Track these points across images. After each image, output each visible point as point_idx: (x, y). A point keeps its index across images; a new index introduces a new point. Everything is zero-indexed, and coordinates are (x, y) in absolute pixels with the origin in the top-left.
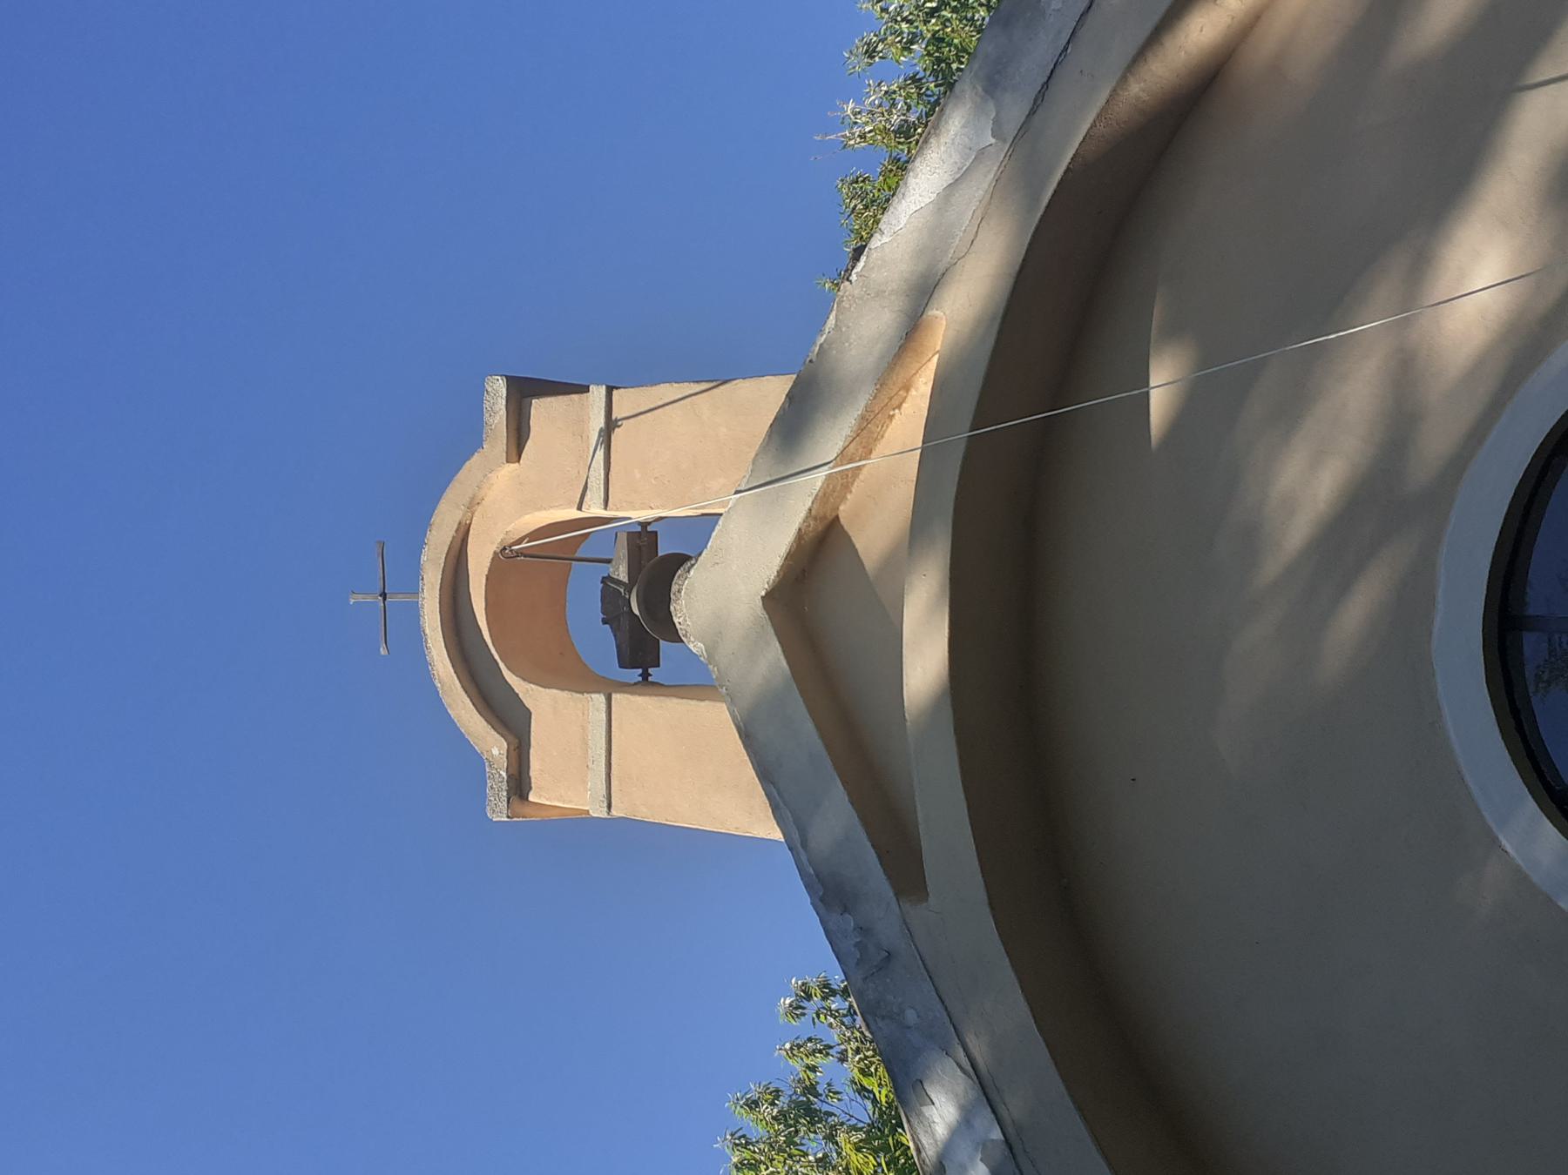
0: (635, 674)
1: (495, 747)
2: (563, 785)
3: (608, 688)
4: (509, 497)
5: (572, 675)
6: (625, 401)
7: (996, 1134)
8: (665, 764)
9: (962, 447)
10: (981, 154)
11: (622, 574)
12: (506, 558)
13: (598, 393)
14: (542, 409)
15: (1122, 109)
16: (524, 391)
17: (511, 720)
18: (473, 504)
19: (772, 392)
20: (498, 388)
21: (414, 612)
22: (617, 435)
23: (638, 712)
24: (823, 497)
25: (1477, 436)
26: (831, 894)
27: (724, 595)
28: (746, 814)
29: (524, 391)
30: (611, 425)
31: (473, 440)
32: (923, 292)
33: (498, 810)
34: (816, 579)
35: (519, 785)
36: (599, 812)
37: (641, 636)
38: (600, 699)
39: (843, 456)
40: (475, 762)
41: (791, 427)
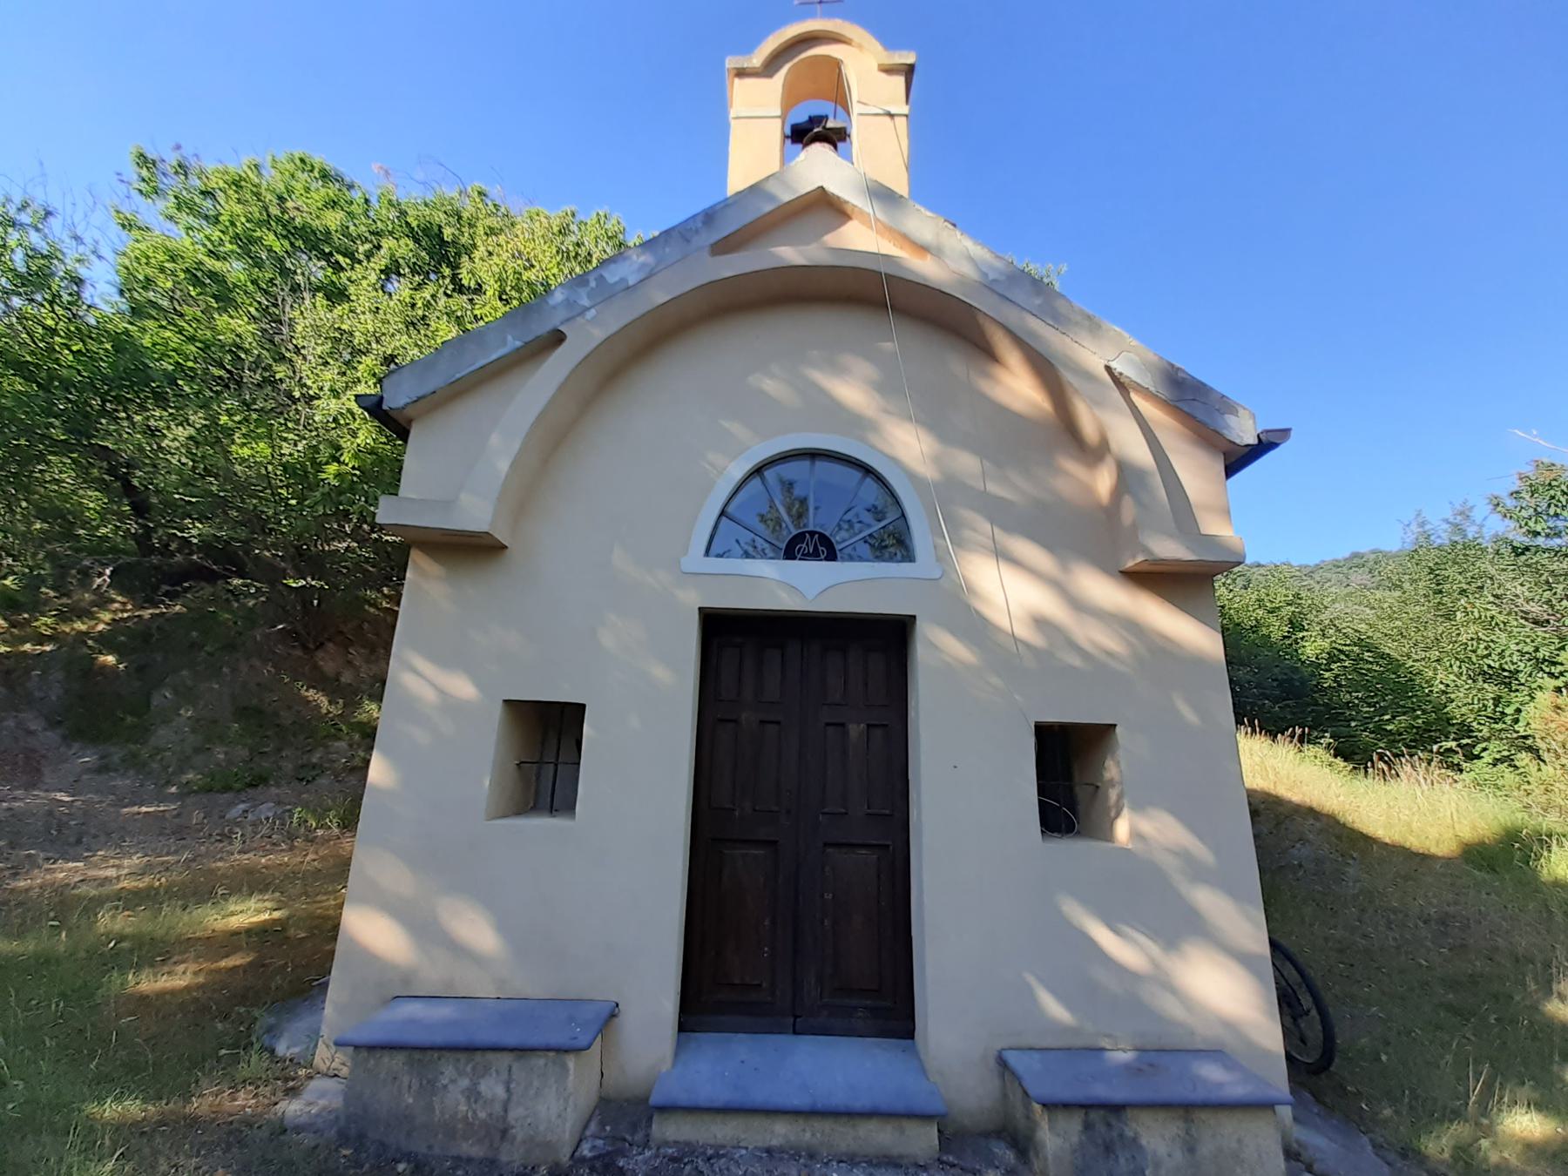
0: (788, 132)
1: (757, 60)
2: (741, 87)
3: (783, 117)
4: (865, 67)
5: (790, 98)
6: (902, 123)
7: (631, 283)
8: (753, 151)
9: (874, 268)
10: (985, 275)
11: (830, 125)
12: (836, 65)
13: (905, 110)
14: (899, 81)
15: (981, 319)
16: (909, 71)
17: (770, 67)
18: (860, 47)
19: (901, 186)
20: (910, 58)
21: (813, 15)
22: (887, 119)
23: (774, 132)
24: (861, 212)
25: (873, 447)
26: (709, 217)
27: (817, 168)
28: (737, 181)
29: (909, 71)
30: (891, 116)
31: (889, 44)
32: (923, 249)
33: (731, 62)
34: (825, 207)
35: (741, 73)
36: (732, 114)
37: (802, 134)
38: (778, 113)
39: (877, 220)
40: (748, 48)
41: (882, 194)
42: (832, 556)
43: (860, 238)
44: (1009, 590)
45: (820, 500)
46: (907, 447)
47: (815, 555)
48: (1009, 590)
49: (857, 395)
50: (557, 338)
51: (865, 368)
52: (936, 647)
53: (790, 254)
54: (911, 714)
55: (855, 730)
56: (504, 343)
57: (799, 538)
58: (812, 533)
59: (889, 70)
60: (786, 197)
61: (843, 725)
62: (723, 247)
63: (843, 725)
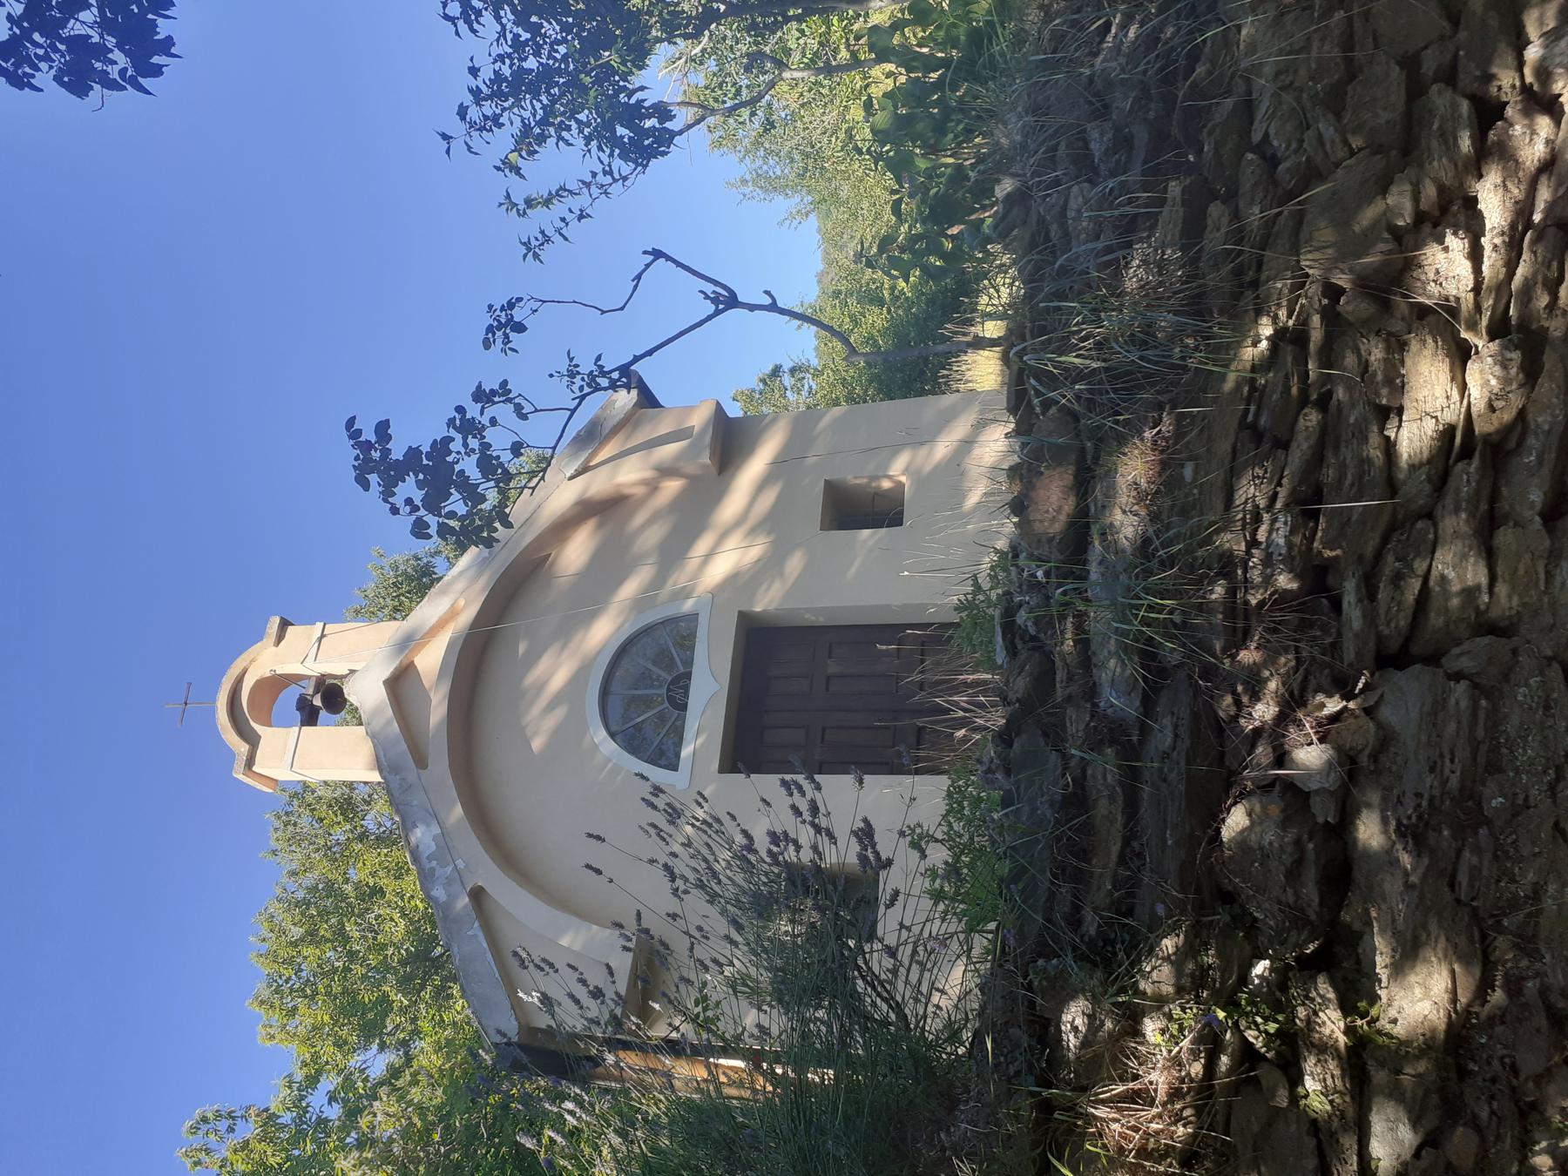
1: (242, 748)
4: (267, 659)
6: (330, 628)
12: (260, 684)
13: (320, 625)
17: (252, 740)
18: (253, 660)
29: (285, 624)
30: (323, 636)
31: (259, 636)
34: (401, 683)
35: (250, 762)
40: (231, 755)
42: (688, 676)
43: (430, 660)
44: (722, 560)
45: (641, 687)
46: (603, 632)
47: (686, 689)
48: (722, 560)
49: (559, 670)
50: (477, 895)
51: (533, 658)
52: (767, 601)
53: (437, 710)
54: (811, 619)
55: (833, 668)
56: (475, 936)
57: (671, 700)
58: (669, 690)
59: (280, 637)
60: (389, 712)
61: (828, 678)
62: (421, 762)
63: (828, 678)
